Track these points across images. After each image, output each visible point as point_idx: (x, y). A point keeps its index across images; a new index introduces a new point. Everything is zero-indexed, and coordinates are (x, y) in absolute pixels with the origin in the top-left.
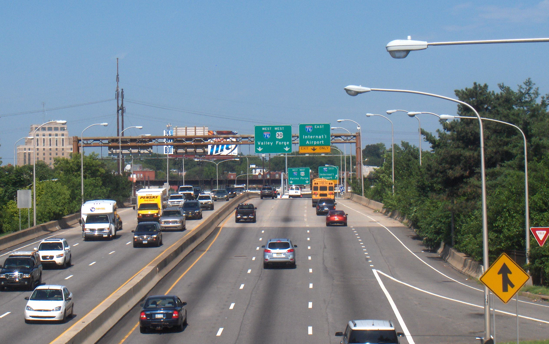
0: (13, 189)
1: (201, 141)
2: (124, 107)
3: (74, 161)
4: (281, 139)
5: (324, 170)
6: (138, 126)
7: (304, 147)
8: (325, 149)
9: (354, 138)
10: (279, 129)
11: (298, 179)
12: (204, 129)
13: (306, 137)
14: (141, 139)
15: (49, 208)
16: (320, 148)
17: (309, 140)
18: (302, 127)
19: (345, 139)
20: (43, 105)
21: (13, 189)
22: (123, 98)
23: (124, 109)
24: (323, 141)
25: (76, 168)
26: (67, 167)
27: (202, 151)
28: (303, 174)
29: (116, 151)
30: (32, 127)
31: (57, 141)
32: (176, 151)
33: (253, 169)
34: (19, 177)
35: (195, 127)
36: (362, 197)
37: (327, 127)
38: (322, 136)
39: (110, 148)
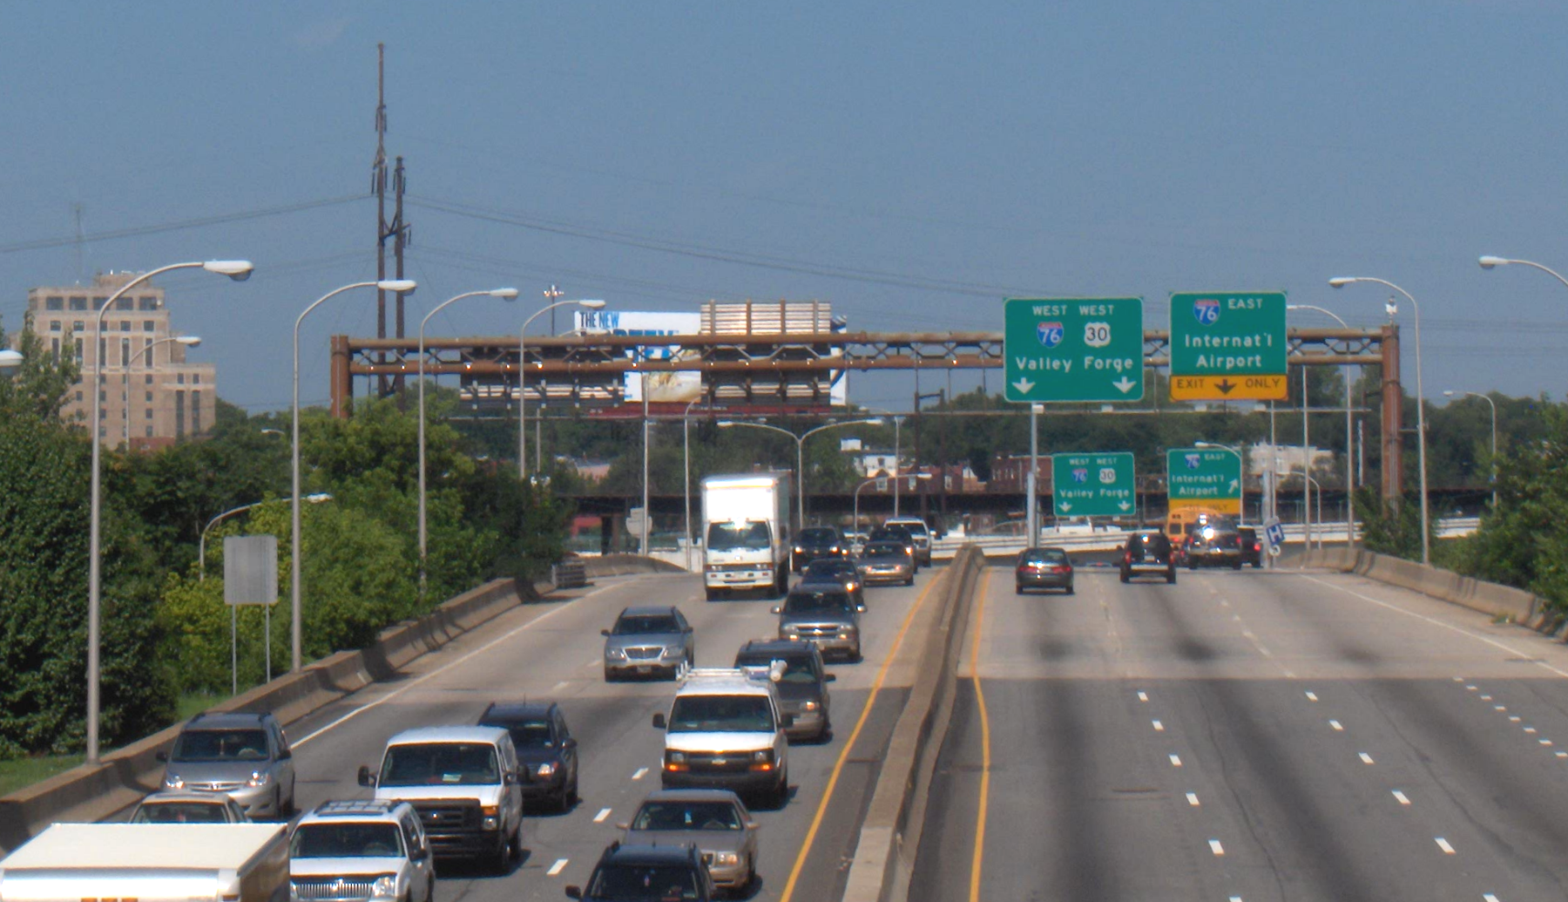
0: (147, 532)
1: (803, 354)
2: (405, 223)
3: (362, 430)
6: (588, 298)
7: (1189, 378)
8: (1266, 386)
9: (1375, 346)
10: (1097, 310)
11: (1091, 494)
12: (815, 311)
13: (1236, 342)
14: (583, 346)
15: (333, 605)
16: (1249, 383)
17: (1208, 351)
18: (1183, 307)
19: (1339, 350)
20: (78, 212)
21: (147, 532)
22: (404, 191)
23: (406, 231)
24: (1258, 358)
25: (367, 455)
26: (338, 451)
27: (809, 392)
28: (1107, 476)
29: (489, 392)
30: (34, 295)
31: (126, 347)
32: (711, 393)
33: (854, 453)
34: (168, 488)
35: (783, 304)
36: (1421, 565)
37: (1274, 303)
38: (1257, 338)
39: (467, 378)
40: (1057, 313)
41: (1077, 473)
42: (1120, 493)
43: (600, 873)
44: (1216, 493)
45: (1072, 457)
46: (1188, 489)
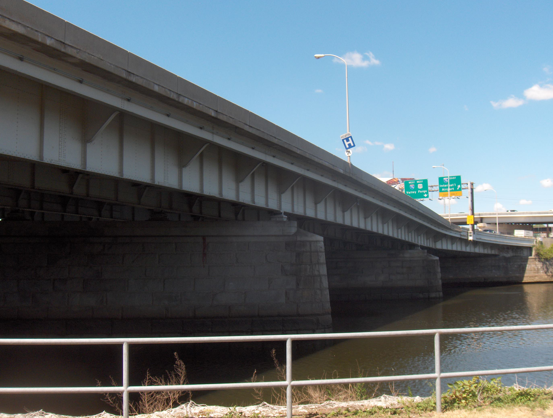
4: (421, 189)
5: (444, 180)
10: (420, 182)
11: (415, 192)
38: (453, 184)
40: (413, 183)
41: (411, 186)
42: (424, 192)
43: (155, 385)
44: (453, 190)
45: (410, 181)
46: (445, 189)
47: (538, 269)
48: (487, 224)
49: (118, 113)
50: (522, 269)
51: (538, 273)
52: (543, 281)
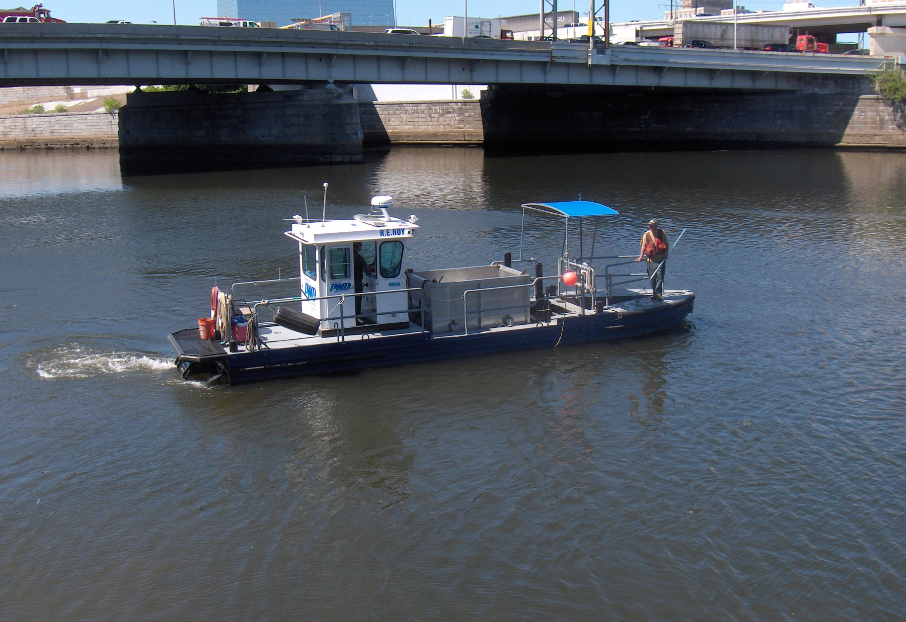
47: (882, 121)
48: (891, 27)
49: (188, 364)
50: (844, 118)
51: (881, 128)
52: (889, 144)
